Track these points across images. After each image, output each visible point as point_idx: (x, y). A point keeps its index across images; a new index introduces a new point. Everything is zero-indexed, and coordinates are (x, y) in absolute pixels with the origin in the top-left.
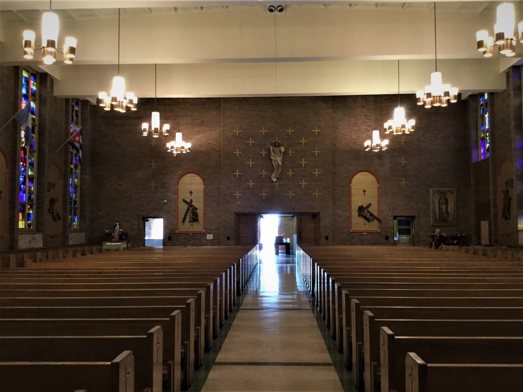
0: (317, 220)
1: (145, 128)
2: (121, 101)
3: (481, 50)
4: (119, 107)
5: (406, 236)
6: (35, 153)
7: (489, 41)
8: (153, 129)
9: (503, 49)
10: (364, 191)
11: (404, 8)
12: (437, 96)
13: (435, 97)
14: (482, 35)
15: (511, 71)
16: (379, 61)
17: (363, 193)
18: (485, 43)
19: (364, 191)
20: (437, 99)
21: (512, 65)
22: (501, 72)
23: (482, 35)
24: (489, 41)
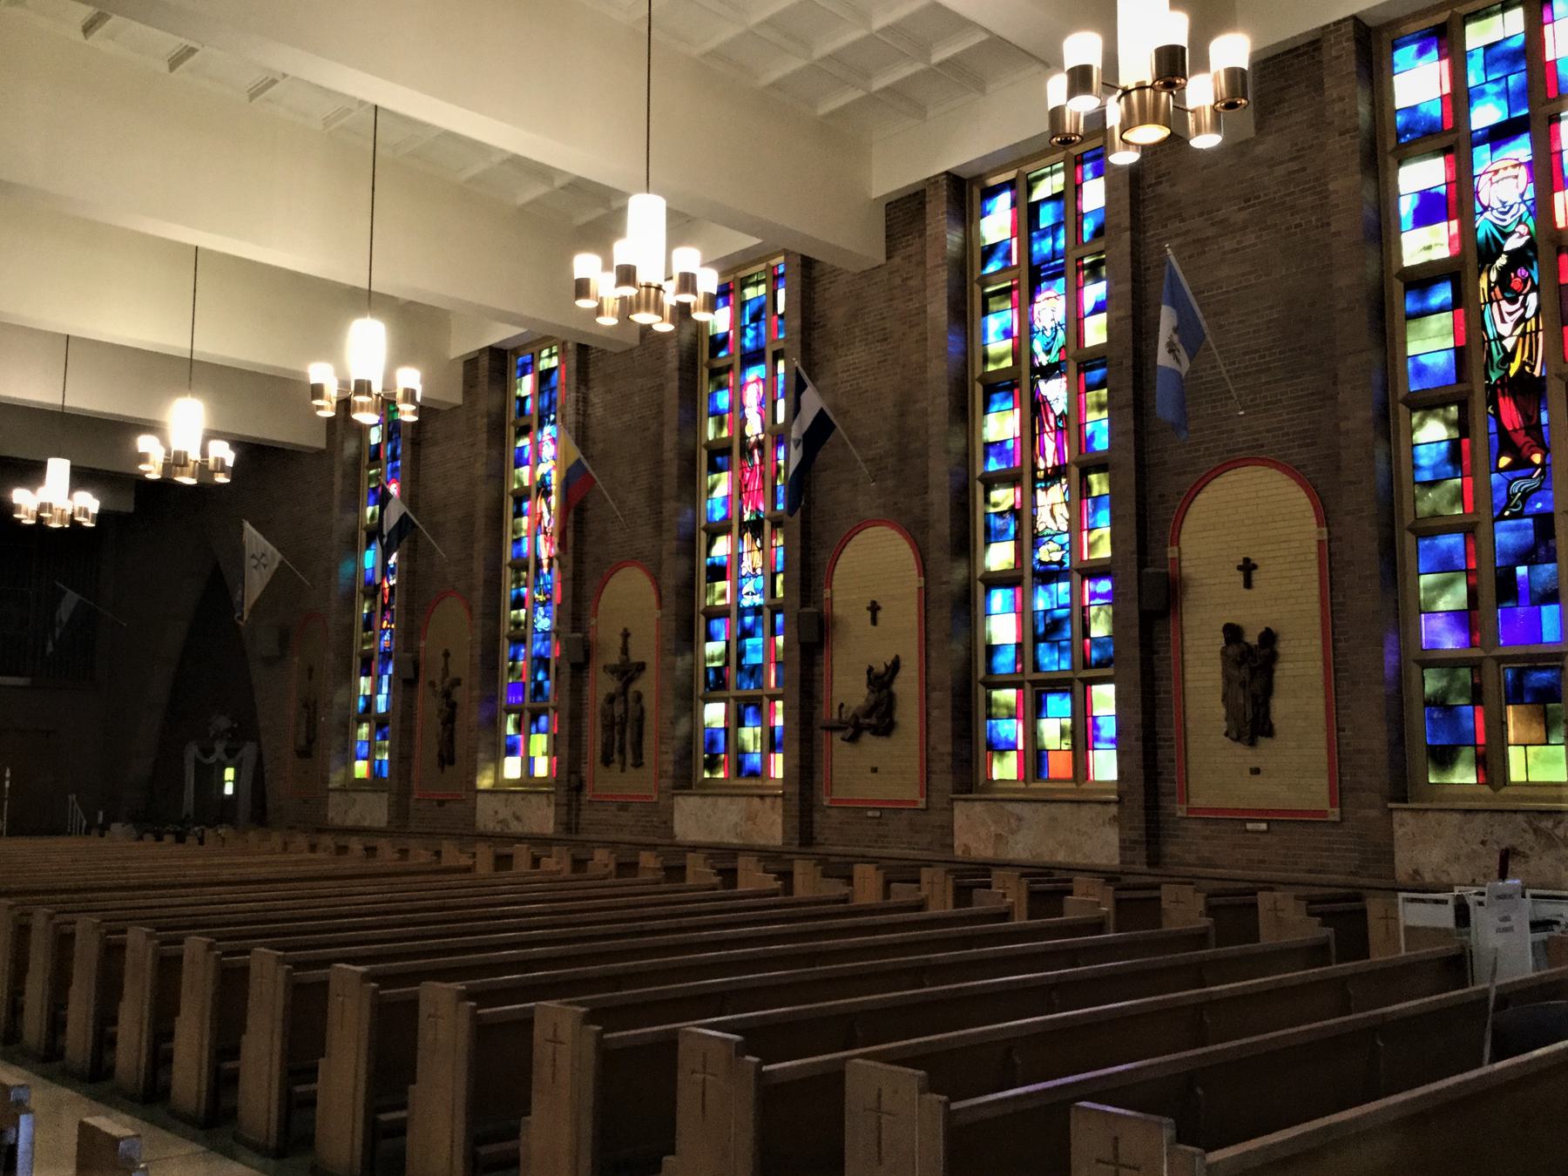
0: (658, 883)
1: (183, 449)
2: (655, 284)
3: (583, 304)
4: (647, 309)
5: (127, 1118)
6: (507, 631)
7: (606, 289)
8: (211, 461)
9: (638, 309)
10: (1248, 568)
11: (256, 100)
12: (648, 286)
13: (644, 289)
14: (585, 265)
15: (485, 362)
16: (145, 237)
17: (1239, 577)
18: (593, 287)
19: (1248, 568)
20: (648, 294)
21: (487, 344)
22: (452, 357)
23: (585, 265)
24: (606, 289)
